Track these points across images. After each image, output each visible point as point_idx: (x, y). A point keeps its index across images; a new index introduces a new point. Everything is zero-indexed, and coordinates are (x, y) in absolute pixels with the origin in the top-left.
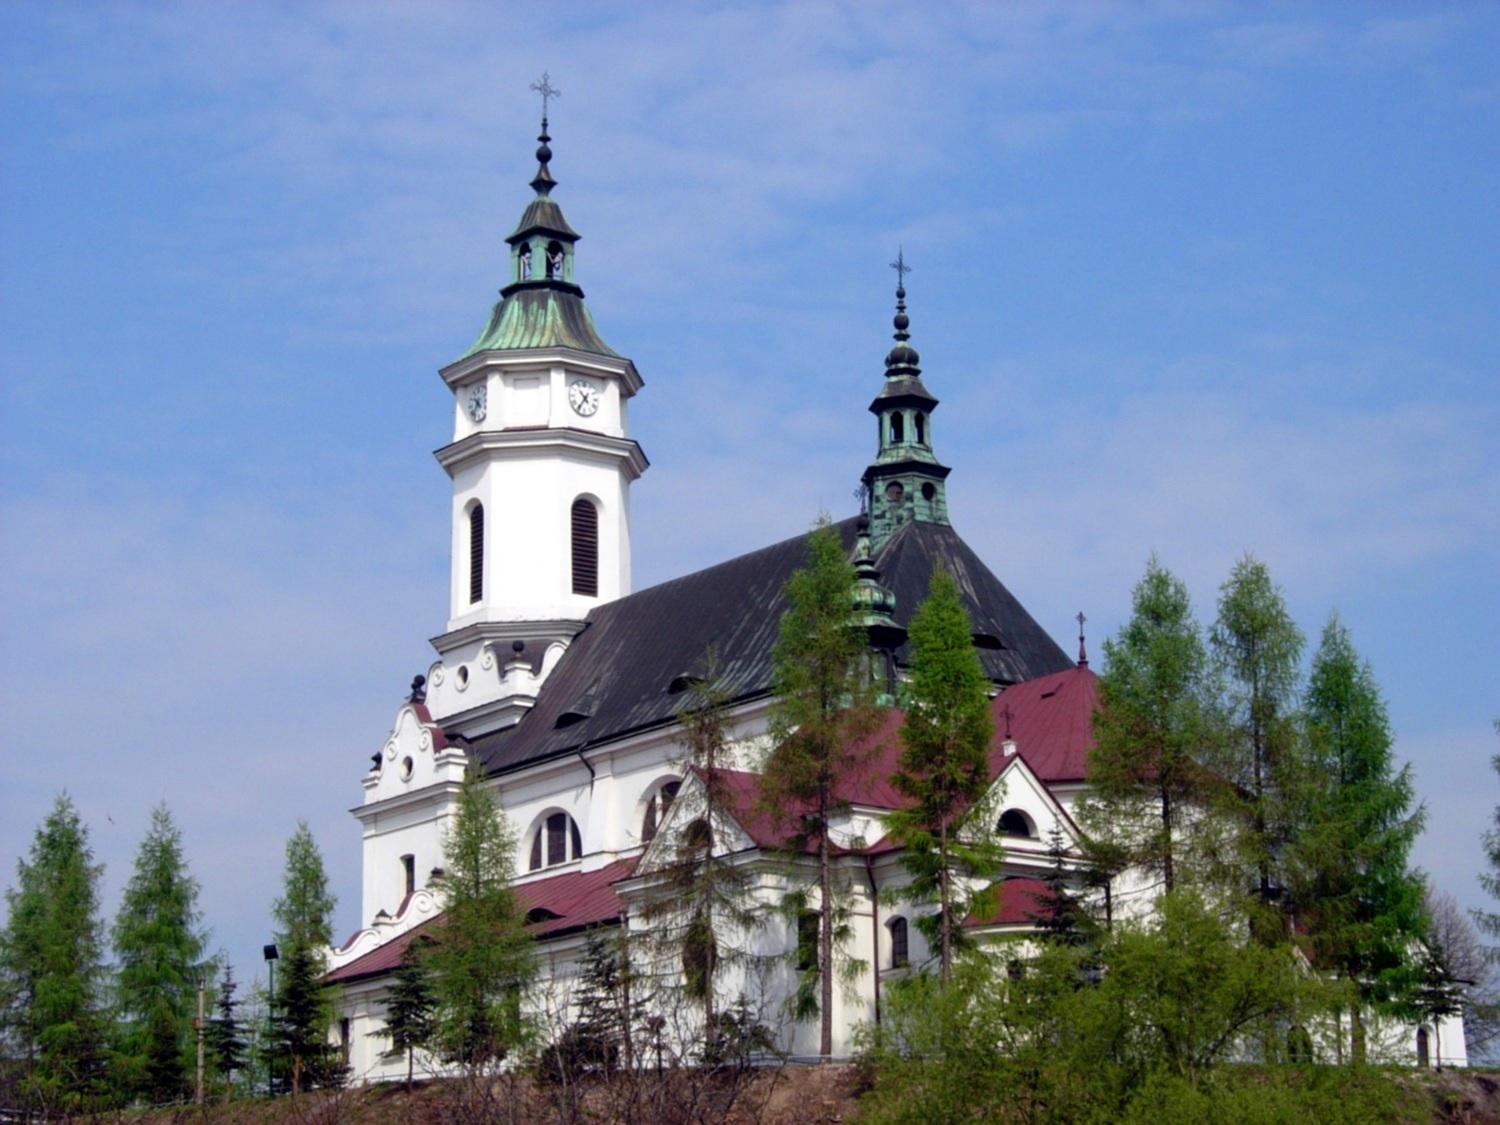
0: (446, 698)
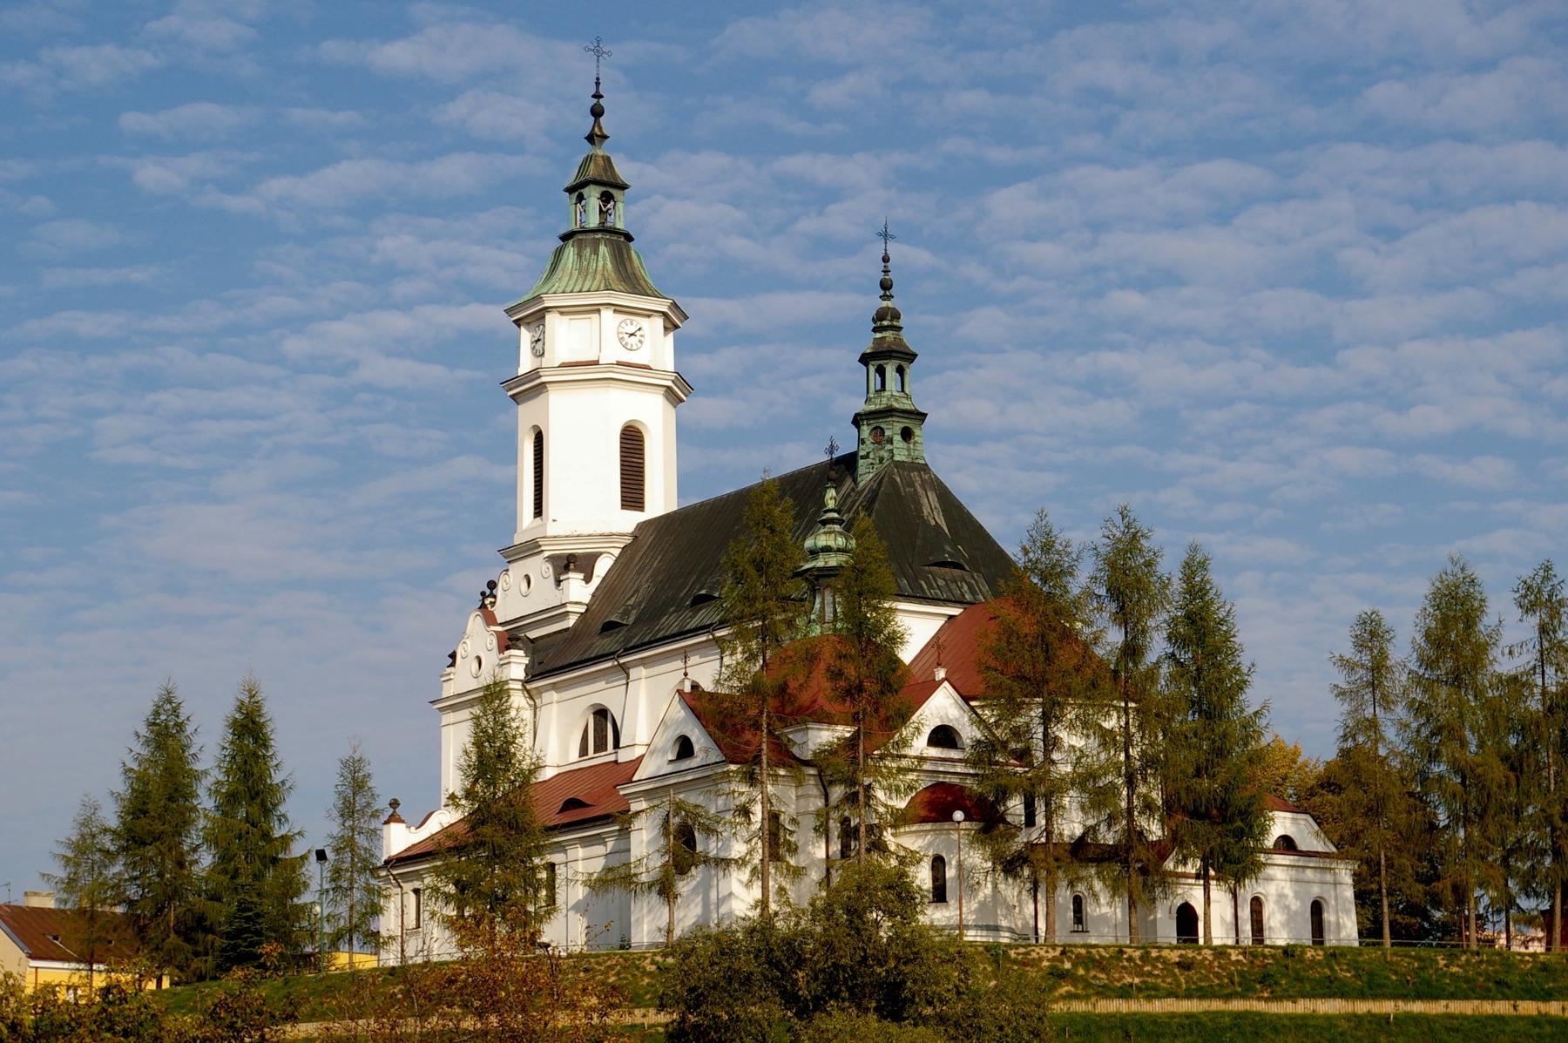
0: (509, 606)
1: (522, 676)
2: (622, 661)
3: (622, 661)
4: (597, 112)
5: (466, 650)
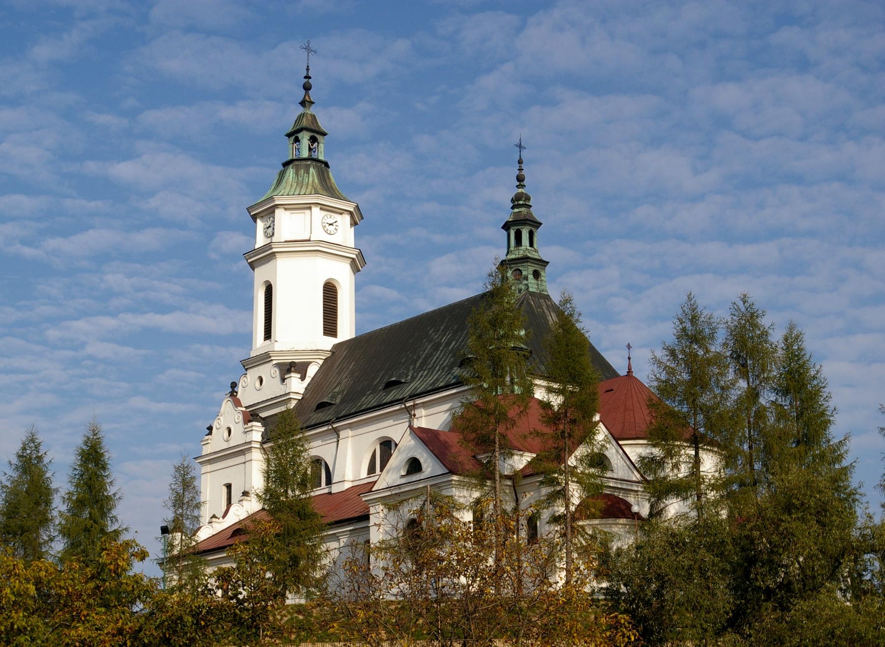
0: (249, 394)
1: (260, 439)
2: (335, 426)
3: (335, 426)
4: (307, 88)
5: (220, 425)
